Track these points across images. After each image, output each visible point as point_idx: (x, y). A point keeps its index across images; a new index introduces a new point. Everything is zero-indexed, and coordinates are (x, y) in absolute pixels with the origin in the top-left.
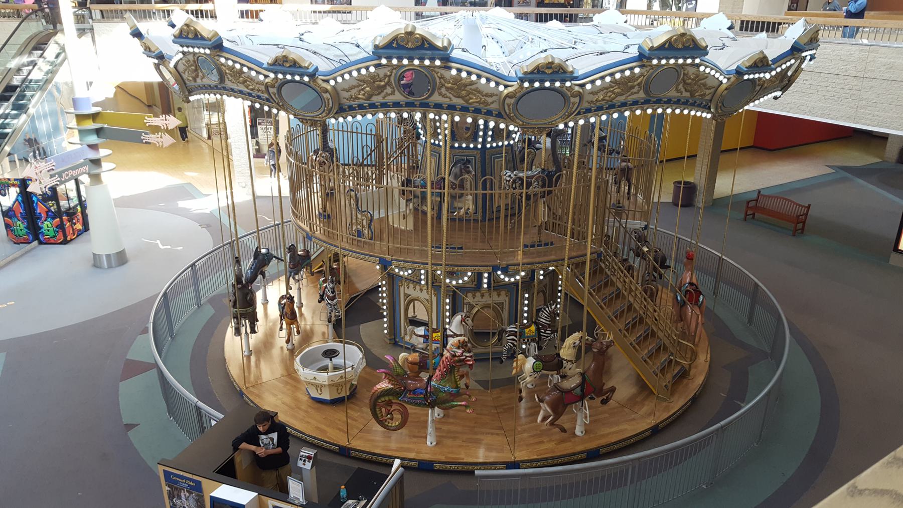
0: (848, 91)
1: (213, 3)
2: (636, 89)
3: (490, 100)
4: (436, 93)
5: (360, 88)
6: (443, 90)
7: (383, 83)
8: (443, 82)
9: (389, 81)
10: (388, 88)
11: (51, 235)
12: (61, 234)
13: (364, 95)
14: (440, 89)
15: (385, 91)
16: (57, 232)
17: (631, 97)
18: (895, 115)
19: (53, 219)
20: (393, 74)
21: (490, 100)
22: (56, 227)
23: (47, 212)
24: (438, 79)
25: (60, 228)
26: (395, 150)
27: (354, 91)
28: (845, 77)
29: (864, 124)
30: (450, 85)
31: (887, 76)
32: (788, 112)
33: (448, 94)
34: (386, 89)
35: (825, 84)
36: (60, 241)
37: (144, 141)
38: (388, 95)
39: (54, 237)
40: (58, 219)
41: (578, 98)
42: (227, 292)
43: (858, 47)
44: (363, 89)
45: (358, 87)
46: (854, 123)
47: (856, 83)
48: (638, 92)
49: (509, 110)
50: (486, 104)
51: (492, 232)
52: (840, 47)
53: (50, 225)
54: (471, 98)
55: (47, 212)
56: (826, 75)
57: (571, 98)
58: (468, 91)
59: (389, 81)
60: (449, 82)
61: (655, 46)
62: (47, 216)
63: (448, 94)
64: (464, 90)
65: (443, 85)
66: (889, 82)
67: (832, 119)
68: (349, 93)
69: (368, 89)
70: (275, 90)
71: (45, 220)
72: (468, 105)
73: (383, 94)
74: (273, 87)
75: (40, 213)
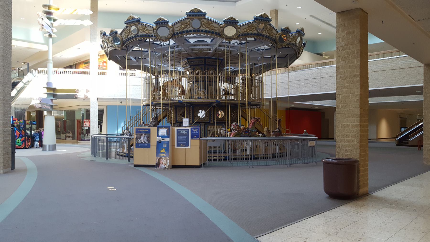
0: (317, 83)
1: (40, 147)
2: (254, 30)
3: (216, 29)
4: (202, 27)
5: (181, 26)
6: (204, 26)
7: (187, 24)
8: (204, 23)
9: (189, 23)
10: (189, 26)
11: (19, 145)
12: (24, 144)
13: (182, 29)
14: (203, 25)
15: (188, 27)
16: (22, 143)
17: (253, 32)
18: (332, 87)
19: (22, 137)
20: (190, 21)
21: (216, 29)
22: (22, 141)
23: (19, 135)
24: (202, 22)
25: (24, 142)
26: (159, 113)
27: (179, 28)
28: (315, 79)
29: (324, 92)
30: (206, 24)
31: (327, 76)
32: (299, 94)
33: (205, 27)
34: (188, 26)
35: (309, 83)
36: (22, 147)
37: (75, 97)
38: (188, 28)
39: (20, 145)
40: (24, 138)
41: (240, 29)
42: (126, 98)
43: (317, 69)
44: (181, 27)
45: (180, 26)
46: (320, 92)
47: (318, 80)
48: (255, 31)
49: (221, 32)
50: (215, 30)
51: (211, 85)
52: (311, 70)
53: (20, 140)
54: (211, 28)
55: (19, 135)
56: (309, 80)
57: (238, 29)
58: (210, 26)
59: (189, 23)
60: (205, 23)
61: (258, 16)
62: (19, 136)
63: (205, 27)
64: (209, 25)
65: (204, 24)
66: (328, 78)
67: (313, 93)
68: (177, 29)
69: (183, 26)
70: (155, 31)
71: (18, 138)
72: (210, 31)
73: (187, 28)
74: (155, 30)
75: (16, 135)
